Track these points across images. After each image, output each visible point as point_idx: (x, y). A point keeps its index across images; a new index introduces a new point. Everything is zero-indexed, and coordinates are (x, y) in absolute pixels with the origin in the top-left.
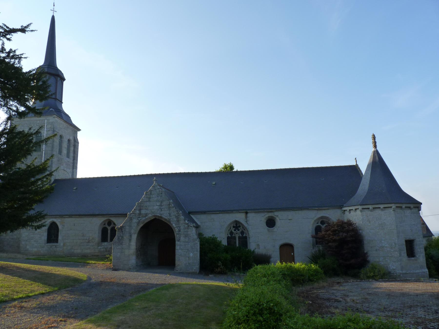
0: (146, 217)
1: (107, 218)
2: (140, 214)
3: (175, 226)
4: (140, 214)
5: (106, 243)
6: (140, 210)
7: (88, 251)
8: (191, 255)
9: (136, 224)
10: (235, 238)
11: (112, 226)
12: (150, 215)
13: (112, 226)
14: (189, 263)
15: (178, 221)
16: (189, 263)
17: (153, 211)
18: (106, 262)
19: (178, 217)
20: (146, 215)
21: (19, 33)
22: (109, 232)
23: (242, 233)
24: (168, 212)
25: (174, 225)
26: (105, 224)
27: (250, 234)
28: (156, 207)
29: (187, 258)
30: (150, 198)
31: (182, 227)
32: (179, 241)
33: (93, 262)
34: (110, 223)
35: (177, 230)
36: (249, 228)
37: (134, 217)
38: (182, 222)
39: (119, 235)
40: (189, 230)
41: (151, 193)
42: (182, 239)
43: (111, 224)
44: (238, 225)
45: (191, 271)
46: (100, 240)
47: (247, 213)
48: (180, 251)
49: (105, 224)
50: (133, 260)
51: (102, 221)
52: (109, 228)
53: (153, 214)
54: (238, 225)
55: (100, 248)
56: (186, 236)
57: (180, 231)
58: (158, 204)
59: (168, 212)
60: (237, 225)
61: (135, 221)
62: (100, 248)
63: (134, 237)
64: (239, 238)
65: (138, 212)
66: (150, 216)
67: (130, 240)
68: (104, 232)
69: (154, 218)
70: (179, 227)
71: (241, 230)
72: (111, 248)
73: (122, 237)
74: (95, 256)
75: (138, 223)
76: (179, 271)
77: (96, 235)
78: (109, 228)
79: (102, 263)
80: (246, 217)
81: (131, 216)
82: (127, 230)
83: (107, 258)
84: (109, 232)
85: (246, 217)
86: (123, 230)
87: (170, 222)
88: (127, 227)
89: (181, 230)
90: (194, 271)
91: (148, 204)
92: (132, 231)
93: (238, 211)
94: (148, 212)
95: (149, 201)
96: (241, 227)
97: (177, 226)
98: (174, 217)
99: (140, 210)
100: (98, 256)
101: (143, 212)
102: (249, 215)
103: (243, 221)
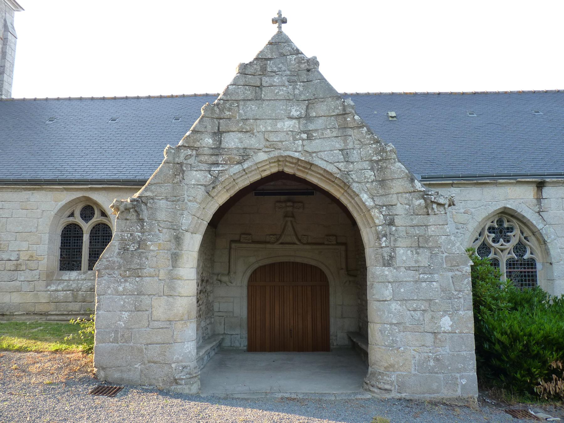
0: (246, 165)
1: (79, 194)
2: (218, 150)
3: (369, 203)
4: (218, 150)
5: (74, 274)
6: (218, 134)
7: (15, 299)
8: (446, 323)
9: (200, 193)
10: (495, 263)
11: (97, 218)
12: (262, 156)
13: (97, 218)
14: (437, 360)
15: (382, 182)
16: (437, 360)
17: (273, 138)
18: (69, 342)
19: (379, 165)
20: (245, 154)
21: (152, 403)
22: (86, 238)
23: (520, 248)
24: (339, 144)
25: (365, 197)
26: (72, 215)
27: (552, 252)
28: (289, 124)
29: (429, 339)
30: (260, 87)
31: (400, 209)
32: (389, 262)
33: (17, 342)
34: (88, 211)
35: (378, 217)
36: (549, 233)
37: (191, 161)
38: (399, 186)
39: (126, 235)
40: (432, 219)
41: (264, 69)
42: (403, 254)
43: (93, 214)
44: (506, 225)
45: (446, 393)
46: (56, 263)
47: (540, 185)
48: (394, 306)
49: (72, 215)
50: (186, 345)
51: (63, 202)
52: (86, 227)
53: (276, 153)
54: (506, 225)
55: (53, 288)
56: (420, 243)
57: (391, 223)
58: (294, 113)
59: (339, 144)
60: (504, 222)
61: (197, 177)
62: (53, 288)
63: (193, 243)
64: (511, 264)
65: (208, 141)
66: (260, 165)
67: (175, 258)
68: (70, 236)
69: (275, 170)
70: (390, 206)
71: (514, 242)
72: (92, 289)
73: (141, 244)
74: (35, 314)
75: (210, 189)
76: (394, 395)
77: (45, 248)
78: (86, 227)
79: (53, 346)
80: (539, 199)
81: (181, 159)
82: (162, 216)
83: (75, 328)
84: (86, 238)
85: (539, 199)
86: (145, 215)
87: (346, 186)
88: (163, 203)
89: (397, 221)
90: (459, 392)
91: (252, 108)
92: (186, 221)
93: (516, 178)
94: (252, 142)
95: (258, 98)
96: (517, 232)
97: (379, 201)
98: (366, 165)
99: (218, 134)
100: (46, 314)
101: (232, 141)
102: (547, 191)
103: (529, 214)
